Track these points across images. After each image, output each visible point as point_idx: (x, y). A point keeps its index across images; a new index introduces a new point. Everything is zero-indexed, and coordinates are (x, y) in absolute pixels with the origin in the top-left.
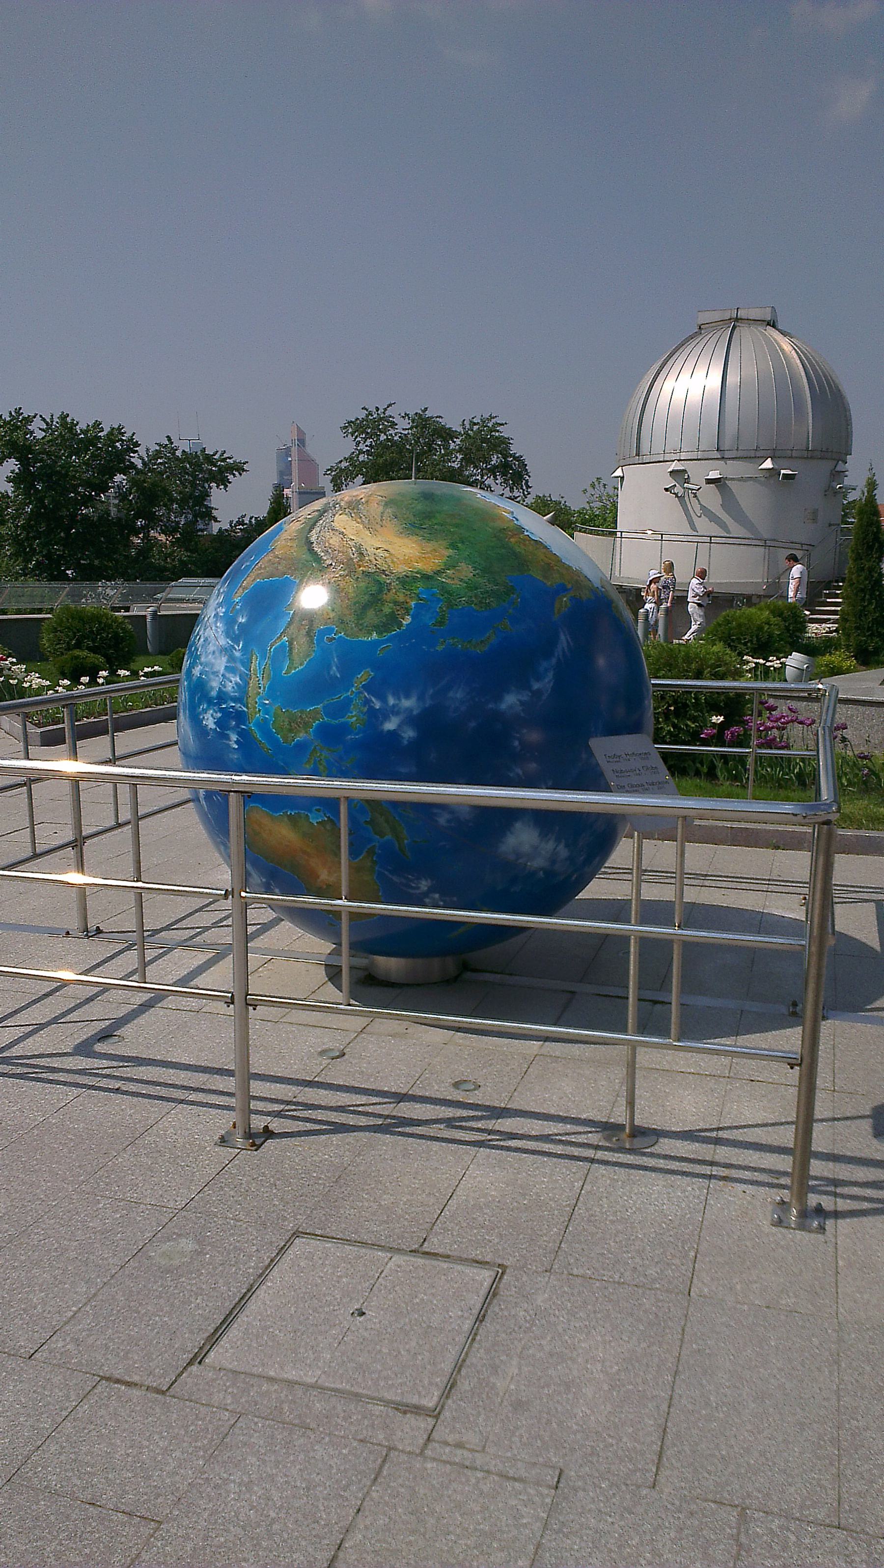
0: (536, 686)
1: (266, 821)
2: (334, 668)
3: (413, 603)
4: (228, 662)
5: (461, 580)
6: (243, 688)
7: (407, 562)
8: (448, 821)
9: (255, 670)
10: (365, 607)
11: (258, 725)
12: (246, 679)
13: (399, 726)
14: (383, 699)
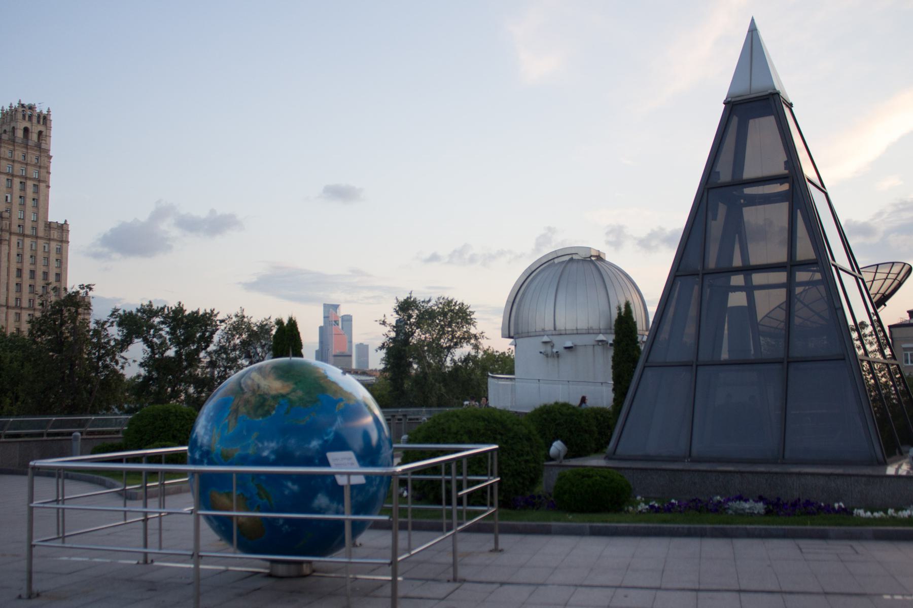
0: (326, 438)
14: (263, 444)
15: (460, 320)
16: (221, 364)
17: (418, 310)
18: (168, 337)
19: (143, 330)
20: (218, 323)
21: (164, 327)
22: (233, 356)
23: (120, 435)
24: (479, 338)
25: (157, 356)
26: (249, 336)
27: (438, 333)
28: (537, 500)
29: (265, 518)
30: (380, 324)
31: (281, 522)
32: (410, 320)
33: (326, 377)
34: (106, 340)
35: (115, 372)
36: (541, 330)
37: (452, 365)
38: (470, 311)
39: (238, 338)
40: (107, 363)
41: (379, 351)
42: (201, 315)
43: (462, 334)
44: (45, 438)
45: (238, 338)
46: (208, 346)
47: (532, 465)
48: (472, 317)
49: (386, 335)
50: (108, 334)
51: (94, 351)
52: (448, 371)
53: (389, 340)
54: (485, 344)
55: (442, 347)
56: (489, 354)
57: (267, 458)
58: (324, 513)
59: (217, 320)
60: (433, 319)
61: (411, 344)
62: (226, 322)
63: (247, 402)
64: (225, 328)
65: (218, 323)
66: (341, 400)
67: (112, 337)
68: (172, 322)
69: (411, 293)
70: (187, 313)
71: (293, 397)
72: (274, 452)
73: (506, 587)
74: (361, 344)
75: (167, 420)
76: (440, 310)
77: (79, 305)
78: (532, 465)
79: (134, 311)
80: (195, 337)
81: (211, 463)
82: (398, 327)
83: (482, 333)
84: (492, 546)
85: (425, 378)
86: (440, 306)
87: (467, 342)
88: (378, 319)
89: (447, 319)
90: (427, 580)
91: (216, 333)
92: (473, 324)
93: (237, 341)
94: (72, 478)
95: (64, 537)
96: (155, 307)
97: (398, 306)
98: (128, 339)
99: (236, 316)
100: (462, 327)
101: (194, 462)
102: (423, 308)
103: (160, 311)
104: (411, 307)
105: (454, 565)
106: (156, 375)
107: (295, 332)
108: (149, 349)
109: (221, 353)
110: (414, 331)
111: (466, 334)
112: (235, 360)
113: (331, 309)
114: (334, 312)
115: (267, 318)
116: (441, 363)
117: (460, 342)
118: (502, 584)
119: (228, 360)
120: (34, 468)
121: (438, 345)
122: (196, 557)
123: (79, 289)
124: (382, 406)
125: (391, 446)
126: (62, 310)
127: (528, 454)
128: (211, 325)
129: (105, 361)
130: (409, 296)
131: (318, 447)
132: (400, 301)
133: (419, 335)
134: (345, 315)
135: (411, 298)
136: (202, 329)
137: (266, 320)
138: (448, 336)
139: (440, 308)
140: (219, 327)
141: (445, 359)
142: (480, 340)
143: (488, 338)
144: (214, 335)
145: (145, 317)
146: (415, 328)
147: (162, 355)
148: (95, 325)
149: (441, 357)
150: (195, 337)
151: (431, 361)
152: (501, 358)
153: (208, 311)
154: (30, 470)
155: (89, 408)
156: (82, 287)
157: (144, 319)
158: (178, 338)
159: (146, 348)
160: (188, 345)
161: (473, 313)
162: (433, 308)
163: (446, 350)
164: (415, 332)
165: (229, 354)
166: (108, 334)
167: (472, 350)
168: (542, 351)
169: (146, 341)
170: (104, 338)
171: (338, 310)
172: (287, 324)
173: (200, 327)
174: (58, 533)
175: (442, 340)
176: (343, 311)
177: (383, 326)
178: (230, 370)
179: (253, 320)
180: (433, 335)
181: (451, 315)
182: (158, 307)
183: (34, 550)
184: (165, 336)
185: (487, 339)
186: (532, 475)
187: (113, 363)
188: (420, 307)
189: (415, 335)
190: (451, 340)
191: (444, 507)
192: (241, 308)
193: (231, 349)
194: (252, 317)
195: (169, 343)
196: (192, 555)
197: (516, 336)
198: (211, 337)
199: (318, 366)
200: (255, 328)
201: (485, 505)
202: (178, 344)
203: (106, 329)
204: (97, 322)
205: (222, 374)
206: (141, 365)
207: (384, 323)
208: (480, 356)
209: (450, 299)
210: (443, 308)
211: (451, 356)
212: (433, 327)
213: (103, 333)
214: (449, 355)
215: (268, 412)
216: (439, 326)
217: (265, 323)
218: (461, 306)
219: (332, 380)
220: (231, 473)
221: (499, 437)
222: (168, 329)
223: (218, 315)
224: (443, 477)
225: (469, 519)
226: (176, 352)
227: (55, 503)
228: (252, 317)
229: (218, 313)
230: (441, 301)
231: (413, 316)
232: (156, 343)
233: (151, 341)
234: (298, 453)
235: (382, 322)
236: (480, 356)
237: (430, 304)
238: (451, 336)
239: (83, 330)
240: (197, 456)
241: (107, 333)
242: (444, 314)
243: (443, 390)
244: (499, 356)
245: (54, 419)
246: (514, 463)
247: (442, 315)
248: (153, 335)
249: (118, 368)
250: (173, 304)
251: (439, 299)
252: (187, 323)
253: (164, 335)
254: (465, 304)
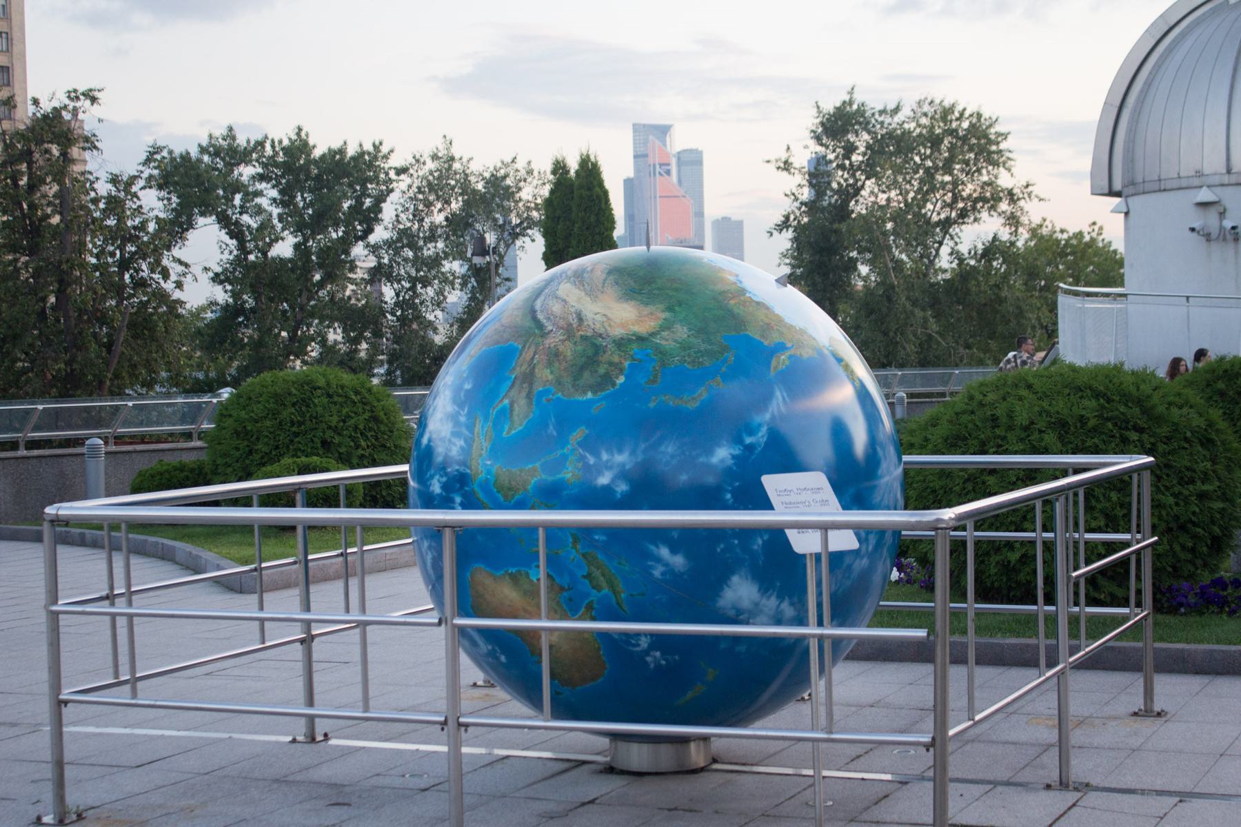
0: (748, 440)
1: (488, 581)
2: (551, 427)
3: (626, 364)
4: (454, 427)
5: (675, 341)
6: (467, 451)
7: (622, 325)
8: (663, 574)
9: (478, 434)
10: (582, 368)
11: (480, 486)
12: (469, 442)
13: (613, 480)
14: (597, 454)
15: (972, 156)
16: (402, 272)
17: (869, 132)
18: (276, 211)
19: (218, 196)
20: (392, 175)
21: (266, 189)
22: (430, 253)
23: (199, 444)
24: (1019, 199)
25: (252, 257)
26: (467, 203)
27: (920, 189)
28: (1230, 590)
29: (604, 635)
30: (778, 168)
31: (644, 643)
32: (849, 159)
33: (743, 291)
34: (137, 221)
35: (162, 296)
36: (1193, 173)
37: (954, 265)
38: (996, 133)
39: (440, 211)
40: (141, 274)
41: (775, 233)
42: (353, 158)
43: (979, 190)
44: (22, 452)
45: (440, 211)
46: (369, 230)
47: (1218, 505)
48: (1003, 146)
49: (793, 194)
50: (141, 207)
51: (111, 248)
52: (944, 280)
53: (799, 209)
54: (1033, 212)
55: (928, 222)
56: (1042, 237)
57: (607, 489)
58: (746, 623)
59: (390, 168)
60: (907, 156)
61: (854, 216)
62: (411, 171)
63: (555, 355)
64: (410, 187)
65: (392, 175)
66: (781, 347)
67: (152, 214)
68: (283, 176)
69: (851, 92)
70: (317, 153)
71: (666, 341)
72: (623, 475)
73: (1197, 803)
74: (726, 219)
75: (308, 406)
76: (924, 131)
77: (69, 140)
78: (1218, 505)
79: (194, 152)
80: (340, 209)
81: (468, 504)
82: (818, 176)
83: (1027, 186)
84: (1139, 703)
85: (889, 299)
86: (924, 121)
87: (990, 209)
88: (772, 158)
89: (941, 154)
90: (995, 783)
91: (388, 199)
92: (1004, 163)
93: (439, 218)
94: (82, 542)
95: (134, 681)
96: (241, 141)
97: (822, 124)
98: (184, 218)
99: (435, 157)
100: (979, 171)
101: (429, 502)
102: (882, 126)
103: (254, 149)
104: (853, 125)
105: (1063, 746)
106: (251, 301)
107: (597, 189)
108: (234, 242)
109: (402, 247)
110: (860, 184)
111: (989, 189)
112: (436, 261)
113: (651, 137)
114: (658, 143)
115: (508, 159)
116: (925, 260)
117: (974, 209)
118: (1184, 796)
119: (418, 262)
120: (56, 521)
121: (918, 215)
122: (454, 726)
123: (67, 101)
124: (874, 363)
125: (900, 459)
126: (30, 153)
127: (1205, 478)
128: (375, 179)
129: (137, 271)
130: (847, 98)
131: (730, 462)
132: (825, 111)
133: (872, 192)
134: (685, 151)
135: (851, 103)
136: (355, 191)
137: (506, 165)
138: (944, 195)
139: (925, 127)
140: (394, 185)
141: (937, 250)
142: (1022, 203)
143: (1042, 197)
144: (383, 205)
145: (220, 165)
146: (863, 178)
147: (265, 254)
148: (110, 186)
149: (926, 247)
150: (340, 211)
151: (904, 257)
152: (1072, 246)
153: (368, 147)
154: (46, 527)
155: (108, 383)
156: (73, 95)
157: (217, 169)
158: (297, 212)
159: (226, 239)
160: (323, 230)
161: (1005, 136)
162: (906, 126)
163: (938, 230)
164: (863, 187)
165: (421, 249)
166: (141, 207)
167: (1002, 228)
168: (1196, 225)
169: (224, 221)
170: (133, 216)
171: (668, 139)
172: (577, 172)
173: (351, 185)
174: (116, 675)
175: (929, 206)
176: (679, 141)
177: (785, 173)
178: (425, 286)
179: (475, 167)
180: (907, 192)
181: (950, 143)
182: (248, 142)
183: (67, 712)
184: (269, 208)
185: (1041, 200)
186: (1216, 530)
187: (156, 276)
188: (874, 126)
189: (863, 193)
190: (951, 206)
191: (1041, 609)
192: (445, 137)
193: (425, 238)
194: (471, 159)
195: (279, 226)
196: (445, 723)
197: (1131, 190)
198: (377, 208)
199: (720, 265)
200: (480, 186)
201: (1125, 603)
202: (299, 228)
203: (135, 195)
204: (114, 180)
205: (407, 297)
206: (217, 279)
207: (787, 166)
208: (1020, 244)
209: (947, 104)
210: (932, 127)
211: (951, 244)
212: (908, 173)
213: (129, 204)
214: (945, 241)
215: (607, 380)
216: (921, 172)
217: (502, 172)
218: (974, 120)
219: (755, 299)
220: (530, 529)
221: (1134, 436)
222: (274, 193)
223: (393, 156)
224: (1038, 535)
225: (1093, 637)
226: (297, 247)
227: (107, 602)
228: (471, 159)
229: (392, 151)
230: (926, 108)
231: (857, 148)
232: (249, 227)
233: (237, 223)
234: (684, 477)
235: (782, 165)
236: (1020, 244)
237: (899, 118)
238: (950, 195)
239: (83, 197)
240: (436, 488)
241: (138, 203)
242: (935, 142)
243: (934, 326)
244: (1067, 241)
245: (40, 407)
246: (1171, 500)
247: (929, 145)
248: (241, 207)
249: (169, 286)
250: (282, 133)
251: (919, 103)
252: (318, 178)
253: (267, 208)
254: (986, 115)
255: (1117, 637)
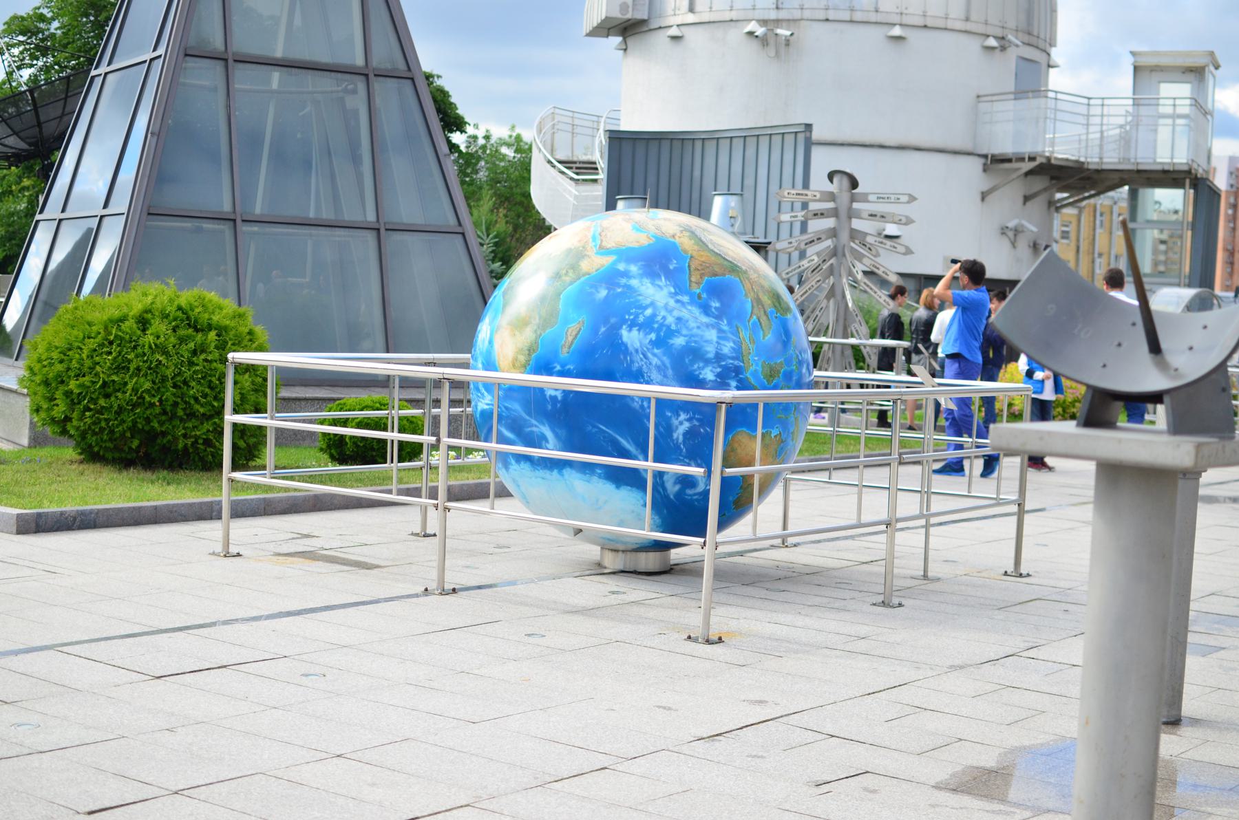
11: (752, 374)
255: (634, 458)
